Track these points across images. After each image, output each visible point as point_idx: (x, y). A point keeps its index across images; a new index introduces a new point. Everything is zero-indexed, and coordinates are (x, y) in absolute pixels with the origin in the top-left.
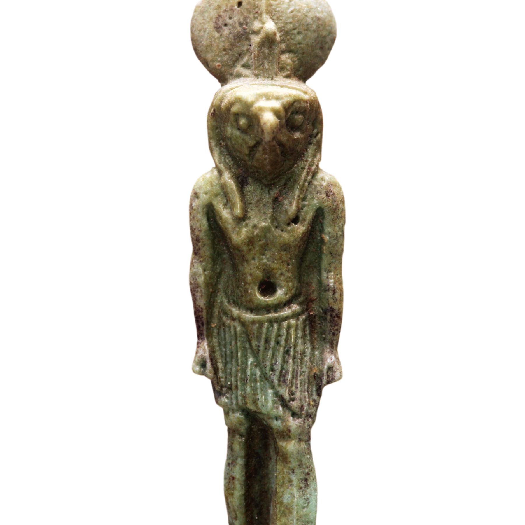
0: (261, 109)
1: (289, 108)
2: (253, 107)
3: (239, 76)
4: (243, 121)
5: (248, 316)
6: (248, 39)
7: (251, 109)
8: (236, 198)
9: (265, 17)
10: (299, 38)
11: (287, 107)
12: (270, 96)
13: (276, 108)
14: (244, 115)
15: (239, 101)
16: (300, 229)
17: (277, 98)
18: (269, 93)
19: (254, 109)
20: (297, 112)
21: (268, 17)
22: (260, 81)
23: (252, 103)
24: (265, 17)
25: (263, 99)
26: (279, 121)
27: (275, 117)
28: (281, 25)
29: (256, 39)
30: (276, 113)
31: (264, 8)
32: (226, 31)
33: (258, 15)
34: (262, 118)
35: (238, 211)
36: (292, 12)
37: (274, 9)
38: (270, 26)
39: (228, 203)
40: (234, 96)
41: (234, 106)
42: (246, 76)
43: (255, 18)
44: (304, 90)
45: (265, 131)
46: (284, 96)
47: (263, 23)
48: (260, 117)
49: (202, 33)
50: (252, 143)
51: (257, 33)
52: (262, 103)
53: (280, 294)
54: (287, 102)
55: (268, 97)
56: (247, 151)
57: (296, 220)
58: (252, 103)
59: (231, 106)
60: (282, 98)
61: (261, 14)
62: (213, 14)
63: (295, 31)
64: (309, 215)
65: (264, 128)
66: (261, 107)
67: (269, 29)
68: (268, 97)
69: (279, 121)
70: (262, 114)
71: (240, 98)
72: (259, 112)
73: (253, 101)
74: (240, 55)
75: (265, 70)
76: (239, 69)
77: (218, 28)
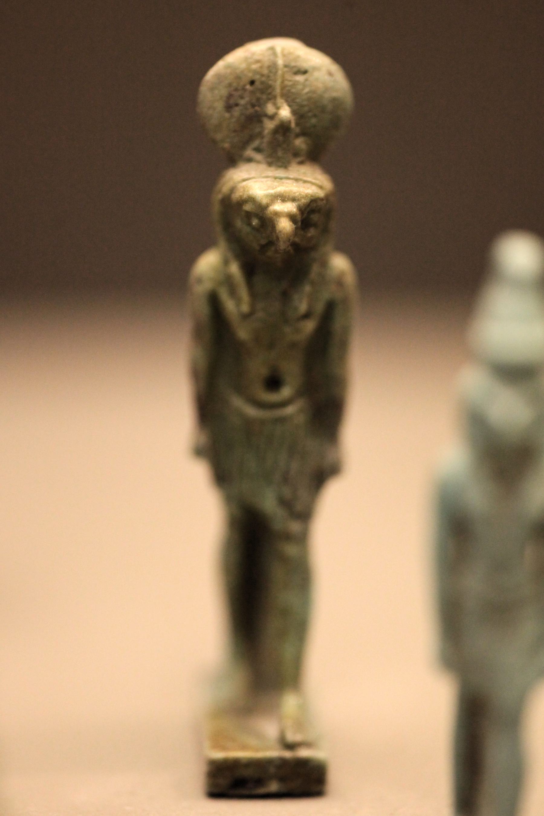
0: (277, 214)
1: (305, 209)
2: (268, 210)
3: (249, 160)
4: (255, 222)
5: (251, 411)
6: (260, 122)
7: (265, 212)
8: (244, 292)
9: (280, 101)
10: (314, 121)
11: (303, 209)
12: (285, 197)
13: (292, 213)
14: (257, 216)
15: (252, 200)
16: (310, 326)
17: (293, 200)
18: (284, 194)
19: (269, 212)
20: (313, 211)
21: (282, 101)
22: (272, 169)
23: (267, 206)
24: (280, 101)
25: (279, 201)
26: (296, 226)
27: (291, 223)
28: (296, 107)
29: (270, 125)
30: (292, 217)
31: (278, 91)
32: (236, 112)
33: (272, 98)
34: (277, 224)
35: (245, 308)
36: (307, 93)
37: (289, 91)
38: (285, 112)
39: (233, 292)
40: (247, 194)
41: (247, 205)
42: (258, 162)
43: (269, 99)
44: (320, 184)
45: (280, 239)
46: (301, 197)
47: (278, 108)
48: (276, 223)
49: (210, 112)
50: (263, 242)
51: (272, 117)
52: (278, 207)
53: (286, 392)
54: (304, 204)
55: (284, 198)
56: (257, 248)
57: (307, 316)
58: (267, 206)
59: (243, 203)
60: (298, 200)
61: (275, 97)
62: (224, 92)
63: (310, 114)
64: (320, 307)
65: (280, 236)
66: (277, 212)
67: (284, 117)
68: (284, 198)
69: (296, 226)
70: (278, 219)
71: (253, 198)
72: (274, 217)
73: (268, 203)
74: (251, 138)
75: (278, 159)
76: (249, 152)
77: (229, 107)
